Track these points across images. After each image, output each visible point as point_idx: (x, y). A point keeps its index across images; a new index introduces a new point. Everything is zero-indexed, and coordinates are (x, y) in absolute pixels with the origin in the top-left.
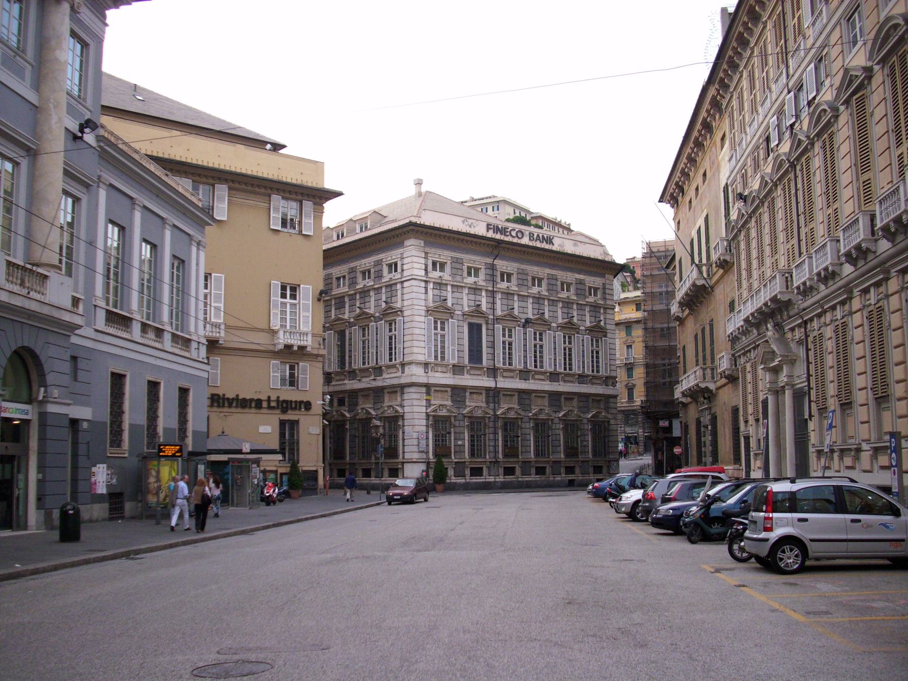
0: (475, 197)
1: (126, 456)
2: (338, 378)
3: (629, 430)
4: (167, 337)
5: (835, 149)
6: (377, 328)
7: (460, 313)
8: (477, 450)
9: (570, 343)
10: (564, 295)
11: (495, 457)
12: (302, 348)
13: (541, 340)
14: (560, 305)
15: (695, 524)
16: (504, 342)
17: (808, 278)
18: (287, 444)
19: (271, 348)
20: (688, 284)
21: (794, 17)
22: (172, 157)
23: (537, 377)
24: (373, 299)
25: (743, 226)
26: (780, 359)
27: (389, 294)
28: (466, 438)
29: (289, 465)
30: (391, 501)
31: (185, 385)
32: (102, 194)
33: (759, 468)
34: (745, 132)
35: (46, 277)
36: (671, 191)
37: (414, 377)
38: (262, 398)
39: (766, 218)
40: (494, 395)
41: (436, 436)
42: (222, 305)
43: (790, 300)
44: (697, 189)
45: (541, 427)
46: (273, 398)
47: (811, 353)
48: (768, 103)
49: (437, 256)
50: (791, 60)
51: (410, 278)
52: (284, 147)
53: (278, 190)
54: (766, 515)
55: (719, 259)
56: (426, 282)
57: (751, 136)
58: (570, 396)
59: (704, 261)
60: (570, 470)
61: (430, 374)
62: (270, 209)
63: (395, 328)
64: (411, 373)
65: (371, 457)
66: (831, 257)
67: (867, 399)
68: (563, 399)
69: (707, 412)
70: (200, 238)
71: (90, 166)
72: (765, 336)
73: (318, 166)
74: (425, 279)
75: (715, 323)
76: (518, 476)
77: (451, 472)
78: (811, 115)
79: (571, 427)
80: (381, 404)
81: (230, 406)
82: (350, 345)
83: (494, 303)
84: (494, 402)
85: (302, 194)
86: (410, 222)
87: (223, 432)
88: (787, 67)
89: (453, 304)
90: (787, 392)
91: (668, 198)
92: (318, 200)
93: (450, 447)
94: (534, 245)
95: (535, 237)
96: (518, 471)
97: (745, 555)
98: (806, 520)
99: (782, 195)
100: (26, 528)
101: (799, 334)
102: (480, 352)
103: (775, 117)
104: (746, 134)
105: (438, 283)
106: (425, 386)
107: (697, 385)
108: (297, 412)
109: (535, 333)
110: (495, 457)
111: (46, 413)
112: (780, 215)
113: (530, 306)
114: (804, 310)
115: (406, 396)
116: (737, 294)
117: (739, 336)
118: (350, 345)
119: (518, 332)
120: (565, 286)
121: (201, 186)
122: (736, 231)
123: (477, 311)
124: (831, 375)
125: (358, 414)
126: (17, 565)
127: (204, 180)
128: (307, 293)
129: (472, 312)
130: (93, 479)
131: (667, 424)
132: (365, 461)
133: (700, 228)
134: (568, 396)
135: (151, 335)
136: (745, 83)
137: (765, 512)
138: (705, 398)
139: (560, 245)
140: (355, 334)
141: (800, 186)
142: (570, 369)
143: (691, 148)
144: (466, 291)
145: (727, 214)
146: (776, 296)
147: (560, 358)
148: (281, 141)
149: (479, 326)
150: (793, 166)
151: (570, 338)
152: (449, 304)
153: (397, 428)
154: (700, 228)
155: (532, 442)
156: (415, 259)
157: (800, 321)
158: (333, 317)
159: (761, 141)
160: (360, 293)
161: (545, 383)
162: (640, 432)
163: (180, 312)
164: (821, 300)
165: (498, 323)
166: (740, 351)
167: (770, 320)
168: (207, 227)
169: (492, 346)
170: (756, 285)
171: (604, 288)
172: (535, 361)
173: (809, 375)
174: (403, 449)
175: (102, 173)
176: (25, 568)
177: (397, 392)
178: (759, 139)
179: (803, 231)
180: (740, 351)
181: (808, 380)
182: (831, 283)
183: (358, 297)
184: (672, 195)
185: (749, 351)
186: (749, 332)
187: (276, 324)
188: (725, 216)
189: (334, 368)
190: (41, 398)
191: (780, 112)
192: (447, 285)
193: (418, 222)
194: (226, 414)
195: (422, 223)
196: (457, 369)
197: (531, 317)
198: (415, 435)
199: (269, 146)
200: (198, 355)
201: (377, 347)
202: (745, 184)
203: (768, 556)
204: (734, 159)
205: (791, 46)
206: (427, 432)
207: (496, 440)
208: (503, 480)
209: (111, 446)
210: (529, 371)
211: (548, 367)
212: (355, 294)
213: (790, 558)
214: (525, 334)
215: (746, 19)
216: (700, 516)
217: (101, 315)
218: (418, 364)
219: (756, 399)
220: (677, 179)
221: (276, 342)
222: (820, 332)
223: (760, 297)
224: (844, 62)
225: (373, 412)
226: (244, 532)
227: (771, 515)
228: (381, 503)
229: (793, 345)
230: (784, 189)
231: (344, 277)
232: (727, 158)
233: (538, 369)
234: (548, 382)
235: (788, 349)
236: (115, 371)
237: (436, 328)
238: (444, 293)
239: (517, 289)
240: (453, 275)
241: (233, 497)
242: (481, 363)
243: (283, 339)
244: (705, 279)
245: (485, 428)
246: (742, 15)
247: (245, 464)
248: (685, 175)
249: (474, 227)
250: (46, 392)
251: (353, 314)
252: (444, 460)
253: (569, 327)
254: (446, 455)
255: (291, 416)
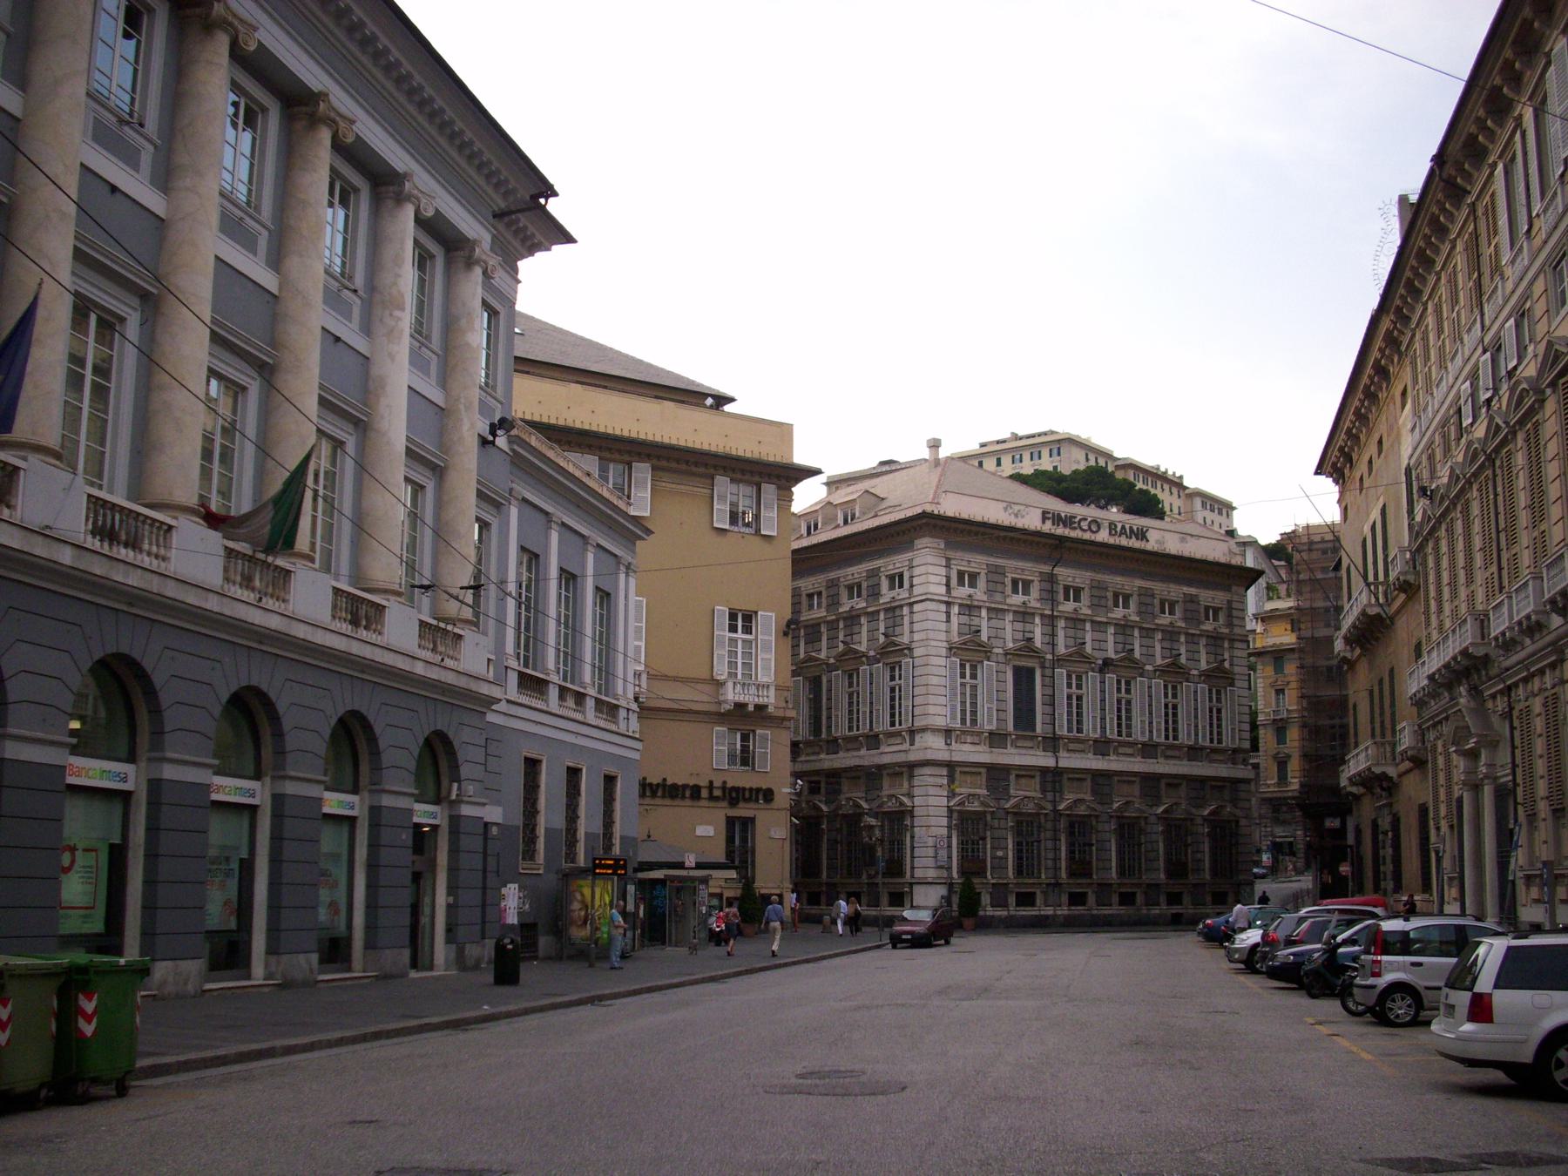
0: (1021, 433)
1: (541, 872)
2: (810, 750)
3: (1279, 831)
4: (590, 703)
5: (1541, 446)
6: (871, 674)
7: (1000, 651)
8: (1027, 865)
9: (1175, 696)
10: (1165, 620)
11: (1055, 877)
12: (760, 708)
13: (1128, 691)
14: (1159, 636)
15: (1315, 973)
16: (1069, 697)
17: (1533, 611)
18: (737, 853)
19: (713, 708)
20: (1356, 612)
21: (1490, 244)
22: (570, 423)
23: (1121, 750)
24: (864, 629)
25: (1431, 532)
26: (1475, 740)
27: (890, 622)
28: (1010, 846)
29: (741, 885)
30: (896, 941)
31: (612, 770)
32: (514, 512)
33: (1455, 899)
34: (1432, 394)
35: (460, 637)
36: (1333, 459)
37: (929, 751)
38: (702, 784)
39: (1459, 525)
40: (1052, 778)
41: (962, 843)
42: (643, 644)
43: (1486, 655)
44: (1370, 462)
45: (1128, 830)
46: (717, 784)
47: (1517, 733)
48: (1459, 360)
49: (964, 563)
50: (1486, 306)
51: (924, 597)
52: (731, 400)
53: (724, 468)
54: (1375, 958)
55: (1398, 579)
56: (948, 604)
57: (1438, 403)
58: (1174, 781)
59: (1381, 577)
60: (1174, 899)
61: (954, 746)
62: (713, 497)
63: (900, 675)
64: (925, 745)
65: (859, 876)
66: (1535, 603)
68: (1163, 786)
69: (1386, 811)
70: (630, 560)
71: (503, 479)
72: (1457, 704)
73: (783, 431)
74: (946, 599)
75: (1396, 671)
76: (1092, 907)
77: (986, 899)
78: (1512, 390)
79: (1176, 830)
80: (878, 792)
81: (654, 795)
82: (829, 699)
83: (1053, 635)
84: (1054, 790)
85: (760, 474)
86: (924, 512)
87: (649, 836)
88: (1482, 315)
89: (989, 638)
90: (1486, 788)
91: (1329, 469)
92: (783, 481)
93: (985, 861)
94: (1117, 542)
95: (1119, 529)
96: (1091, 899)
97: (1360, 1008)
98: (1420, 964)
99: (1479, 498)
100: (431, 968)
101: (1501, 704)
102: (1033, 711)
103: (1468, 382)
104: (1433, 398)
105: (967, 605)
106: (947, 766)
107: (1369, 769)
108: (752, 805)
109: (1119, 682)
110: (1055, 877)
111: (460, 816)
112: (1476, 527)
113: (1111, 639)
114: (1507, 670)
115: (916, 782)
116: (1425, 633)
117: (1426, 699)
118: (829, 699)
119: (1092, 679)
120: (1168, 605)
121: (611, 466)
122: (1424, 537)
123: (1027, 647)
124: (1540, 767)
125: (840, 807)
126: (485, 1007)
127: (617, 456)
128: (768, 623)
129: (1020, 650)
130: (503, 904)
131: (1336, 823)
132: (852, 881)
133: (1374, 523)
134: (1170, 781)
135: (571, 702)
136: (1430, 320)
137: (1374, 954)
138: (1383, 789)
139: (1158, 542)
140: (837, 682)
141: (1499, 489)
142: (1175, 738)
143: (1359, 400)
144: (1010, 617)
145: (1411, 512)
146: (1466, 649)
147: (1159, 722)
148: (724, 389)
149: (1031, 671)
150: (1490, 460)
151: (1174, 688)
152: (984, 637)
153: (902, 829)
154: (1374, 523)
155: (1114, 854)
156: (931, 569)
157: (1502, 686)
158: (802, 655)
159: (1451, 412)
160: (845, 619)
161: (1132, 759)
162: (1296, 834)
163: (605, 671)
164: (1524, 660)
165: (1061, 667)
166: (1428, 720)
167: (1464, 681)
168: (638, 542)
169: (1051, 702)
170: (1448, 623)
171: (1230, 608)
172: (1119, 725)
173: (1514, 766)
174: (912, 862)
175: (514, 485)
176: (493, 1010)
177: (902, 773)
178: (1448, 409)
179: (1505, 556)
180: (1428, 720)
181: (1514, 774)
182: (1537, 636)
183: (841, 625)
184: (1334, 464)
185: (1440, 722)
186: (1439, 695)
187: (721, 672)
188: (1408, 512)
189: (804, 733)
190: (453, 797)
191: (1474, 376)
192: (980, 607)
193: (936, 512)
194: (648, 808)
195: (942, 512)
196: (996, 739)
197: (1113, 656)
198: (931, 842)
199: (709, 401)
200: (628, 727)
201: (871, 703)
202: (1433, 471)
203: (1376, 1005)
204: (1417, 430)
205: (1487, 289)
206: (949, 837)
207: (1056, 849)
208: (1066, 912)
209: (524, 859)
210: (1108, 742)
211: (1139, 735)
212: (837, 620)
213: (1400, 1008)
214: (1102, 682)
216: (1323, 963)
217: (513, 679)
218: (935, 730)
219: (1449, 793)
220: (1341, 443)
221: (721, 698)
222: (1527, 704)
223: (1448, 647)
224: (1550, 327)
225: (865, 805)
226: (713, 979)
227: (1379, 958)
228: (884, 945)
229: (1495, 720)
230: (1480, 490)
231: (820, 594)
232: (1409, 426)
233: (1124, 738)
234: (1139, 759)
235: (1487, 724)
236: (529, 755)
237: (963, 676)
238: (976, 621)
239: (1089, 612)
240: (989, 592)
241: (670, 930)
242: (1034, 730)
243: (732, 695)
244: (1381, 606)
245: (1039, 832)
246: (1422, 225)
247: (689, 884)
248: (1353, 437)
249: (1023, 517)
250: (459, 788)
251: (834, 652)
252: (976, 881)
253: (1174, 672)
254: (979, 873)
255: (743, 811)
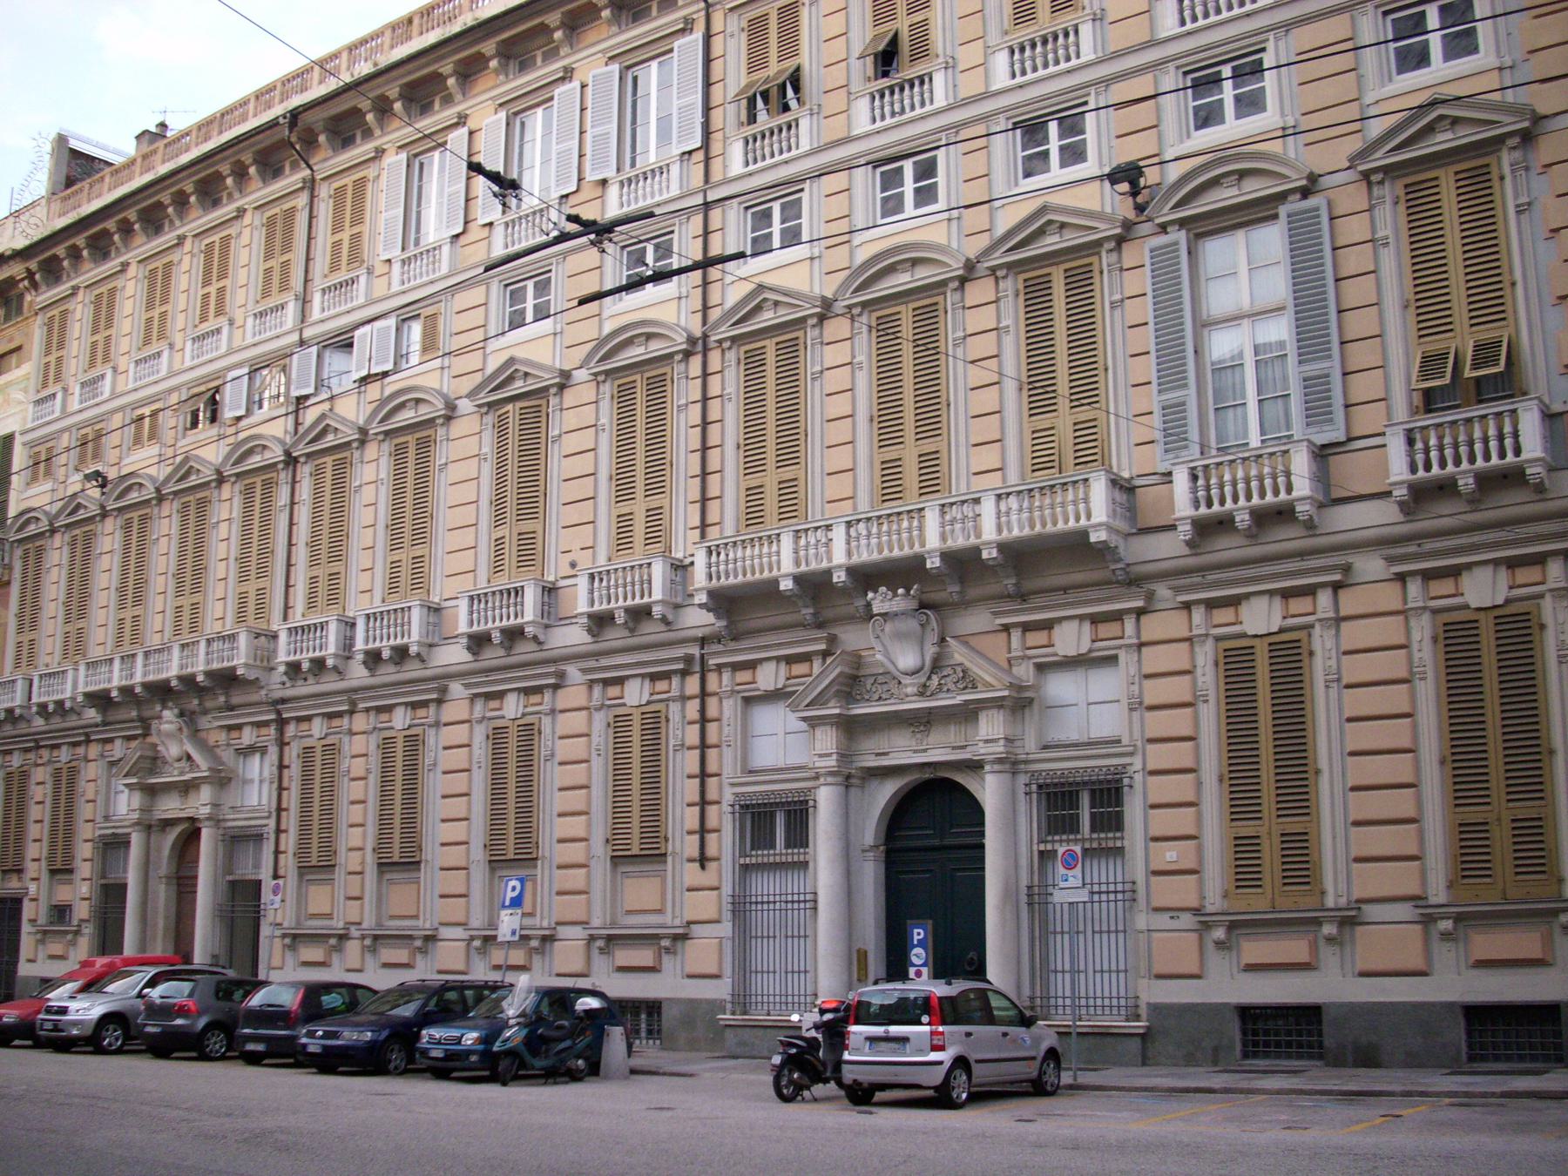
43: (257, 679)
67: (363, 863)
215: (189, 188)
235: (216, 759)
246: (396, 79)
